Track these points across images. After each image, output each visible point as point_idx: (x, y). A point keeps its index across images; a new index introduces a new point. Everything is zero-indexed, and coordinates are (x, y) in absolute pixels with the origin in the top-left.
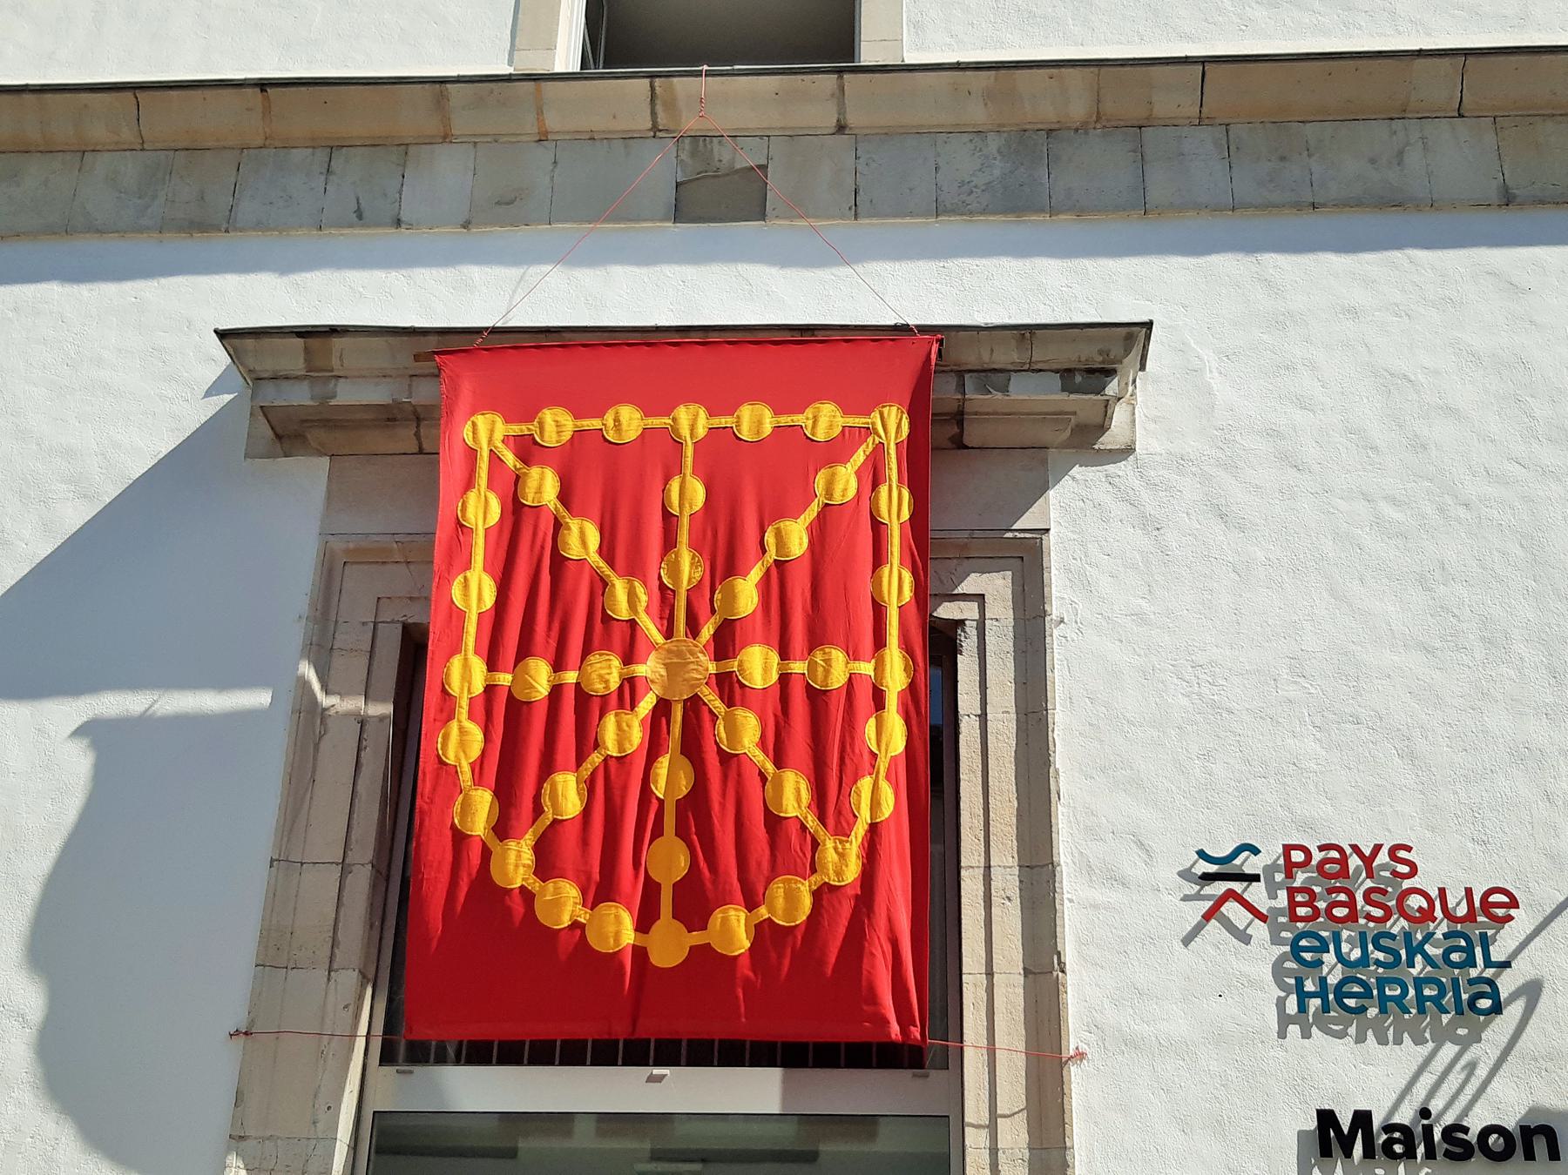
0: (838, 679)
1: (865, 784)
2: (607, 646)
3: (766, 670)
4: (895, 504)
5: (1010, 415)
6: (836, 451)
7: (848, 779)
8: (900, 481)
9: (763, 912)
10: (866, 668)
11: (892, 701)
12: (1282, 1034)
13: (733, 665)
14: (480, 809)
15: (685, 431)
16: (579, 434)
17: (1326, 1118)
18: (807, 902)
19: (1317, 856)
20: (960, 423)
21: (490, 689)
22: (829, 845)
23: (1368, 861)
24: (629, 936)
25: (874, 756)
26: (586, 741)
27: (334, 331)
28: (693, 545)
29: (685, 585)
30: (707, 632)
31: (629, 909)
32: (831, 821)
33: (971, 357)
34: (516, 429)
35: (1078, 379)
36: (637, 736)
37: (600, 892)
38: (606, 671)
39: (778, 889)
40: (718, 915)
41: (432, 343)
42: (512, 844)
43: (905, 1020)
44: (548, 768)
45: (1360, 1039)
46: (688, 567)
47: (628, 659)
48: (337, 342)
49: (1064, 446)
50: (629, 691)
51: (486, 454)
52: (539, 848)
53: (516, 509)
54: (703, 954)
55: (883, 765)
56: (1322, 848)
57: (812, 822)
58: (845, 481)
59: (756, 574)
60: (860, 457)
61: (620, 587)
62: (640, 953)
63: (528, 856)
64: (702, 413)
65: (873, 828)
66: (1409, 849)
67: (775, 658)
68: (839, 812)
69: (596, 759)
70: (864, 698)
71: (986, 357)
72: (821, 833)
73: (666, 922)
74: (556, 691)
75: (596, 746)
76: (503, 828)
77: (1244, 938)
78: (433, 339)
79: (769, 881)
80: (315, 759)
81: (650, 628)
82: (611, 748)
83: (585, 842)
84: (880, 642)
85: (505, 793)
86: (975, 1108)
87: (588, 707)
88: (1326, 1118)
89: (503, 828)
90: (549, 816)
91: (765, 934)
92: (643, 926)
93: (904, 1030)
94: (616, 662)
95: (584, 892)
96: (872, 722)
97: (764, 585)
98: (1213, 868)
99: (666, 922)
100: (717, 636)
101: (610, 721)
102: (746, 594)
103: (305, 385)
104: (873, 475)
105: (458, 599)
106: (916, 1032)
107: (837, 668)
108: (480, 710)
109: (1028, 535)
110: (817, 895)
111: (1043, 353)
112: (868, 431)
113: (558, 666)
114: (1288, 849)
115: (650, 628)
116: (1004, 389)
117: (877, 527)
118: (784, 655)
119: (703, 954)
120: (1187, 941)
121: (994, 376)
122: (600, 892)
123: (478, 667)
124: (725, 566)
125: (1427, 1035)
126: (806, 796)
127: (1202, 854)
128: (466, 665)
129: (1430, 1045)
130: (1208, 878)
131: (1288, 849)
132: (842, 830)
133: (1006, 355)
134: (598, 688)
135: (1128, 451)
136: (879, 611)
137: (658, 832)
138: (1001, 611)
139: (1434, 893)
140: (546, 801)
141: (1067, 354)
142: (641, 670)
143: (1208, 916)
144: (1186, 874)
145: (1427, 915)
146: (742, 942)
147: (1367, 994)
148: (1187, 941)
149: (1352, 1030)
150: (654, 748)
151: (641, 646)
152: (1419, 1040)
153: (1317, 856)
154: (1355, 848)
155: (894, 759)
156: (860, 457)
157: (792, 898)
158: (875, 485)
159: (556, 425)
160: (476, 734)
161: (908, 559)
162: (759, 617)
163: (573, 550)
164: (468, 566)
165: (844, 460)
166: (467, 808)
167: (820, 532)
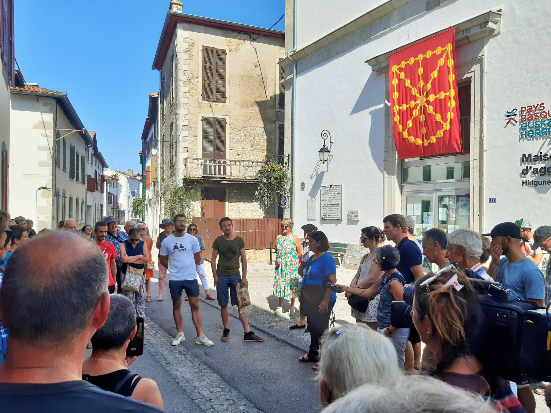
0: (443, 97)
1: (449, 113)
2: (413, 100)
3: (433, 98)
4: (451, 62)
5: (475, 35)
6: (441, 56)
7: (446, 113)
8: (451, 58)
9: (437, 136)
10: (448, 94)
11: (452, 98)
12: (519, 141)
13: (428, 99)
14: (401, 127)
15: (420, 60)
16: (406, 65)
17: (524, 155)
18: (442, 134)
19: (527, 108)
20: (468, 38)
21: (399, 110)
22: (444, 124)
23: (536, 108)
24: (421, 143)
25: (450, 108)
26: (412, 115)
27: (377, 57)
28: (422, 79)
29: (422, 87)
30: (425, 94)
31: (420, 139)
32: (444, 120)
33: (464, 28)
34: (398, 67)
35: (483, 25)
36: (417, 113)
37: (416, 137)
38: (413, 104)
39: (438, 132)
40: (431, 138)
41: (389, 54)
42: (404, 132)
43: (459, 149)
44: (407, 120)
45: (533, 140)
46: (422, 83)
47: (415, 101)
48: (378, 58)
49: (488, 36)
50: (416, 106)
51: (395, 73)
52: (408, 132)
53: (400, 80)
54: (430, 143)
55: (451, 110)
56: (528, 107)
57: (441, 121)
58: (442, 61)
59: (430, 82)
60: (445, 55)
61: (413, 89)
62: (423, 144)
63: (407, 133)
64: (422, 55)
65: (451, 120)
66: (543, 104)
67: (434, 96)
68: (445, 118)
69: (413, 117)
70: (448, 99)
71: (466, 27)
72: (443, 123)
73: (425, 140)
74: (407, 108)
75: (413, 115)
76: (403, 130)
77: (514, 125)
78: (389, 53)
79: (437, 131)
80: (388, 121)
81: (418, 95)
82: (415, 116)
83: (413, 130)
84: (450, 89)
85: (403, 125)
86: (471, 159)
87: (411, 109)
88: (524, 155)
89: (403, 130)
90: (408, 127)
91: (437, 139)
92: (423, 140)
93: (459, 150)
94: (414, 102)
95: (414, 137)
96: (449, 103)
97: (432, 84)
98: (509, 114)
99: (425, 140)
100: (426, 94)
101: (414, 111)
102: (429, 86)
103: (377, 66)
104: (447, 58)
105: (394, 98)
106: (461, 150)
107: (442, 95)
108: (399, 113)
109: (232, 182)
110: (444, 132)
111: (475, 23)
112: (445, 50)
113: (407, 104)
114: (522, 108)
115: (418, 95)
116: (470, 32)
117: (448, 68)
118: (435, 95)
119: (430, 143)
120: (505, 127)
121: (468, 30)
122: (416, 137)
123: (397, 106)
124: (426, 82)
125: (545, 138)
126: (440, 117)
127: (507, 112)
128: (396, 107)
129: (545, 139)
130: (508, 116)
131: (522, 108)
132: (446, 121)
133: (469, 26)
134: (412, 107)
135: (499, 33)
136: (449, 83)
137: (422, 127)
138: (478, 73)
139: (547, 113)
140: (408, 125)
141: (480, 21)
142: (417, 102)
143: (508, 123)
144: (505, 116)
145: (545, 116)
146: (435, 140)
147: (533, 133)
148: (505, 127)
149: (532, 139)
150: (420, 114)
151: (417, 98)
152: (543, 139)
153: (527, 108)
154: (534, 106)
155: (453, 108)
156: (445, 55)
157: (440, 133)
158: (447, 59)
159: (403, 64)
160: (398, 117)
161: (453, 72)
162: (431, 90)
163: (407, 85)
164: (394, 92)
165: (442, 57)
166: (399, 128)
167: (439, 72)
